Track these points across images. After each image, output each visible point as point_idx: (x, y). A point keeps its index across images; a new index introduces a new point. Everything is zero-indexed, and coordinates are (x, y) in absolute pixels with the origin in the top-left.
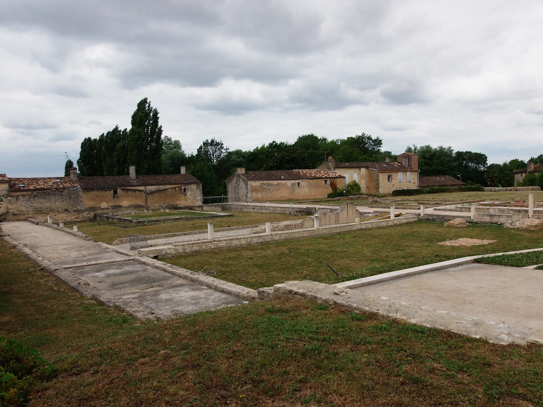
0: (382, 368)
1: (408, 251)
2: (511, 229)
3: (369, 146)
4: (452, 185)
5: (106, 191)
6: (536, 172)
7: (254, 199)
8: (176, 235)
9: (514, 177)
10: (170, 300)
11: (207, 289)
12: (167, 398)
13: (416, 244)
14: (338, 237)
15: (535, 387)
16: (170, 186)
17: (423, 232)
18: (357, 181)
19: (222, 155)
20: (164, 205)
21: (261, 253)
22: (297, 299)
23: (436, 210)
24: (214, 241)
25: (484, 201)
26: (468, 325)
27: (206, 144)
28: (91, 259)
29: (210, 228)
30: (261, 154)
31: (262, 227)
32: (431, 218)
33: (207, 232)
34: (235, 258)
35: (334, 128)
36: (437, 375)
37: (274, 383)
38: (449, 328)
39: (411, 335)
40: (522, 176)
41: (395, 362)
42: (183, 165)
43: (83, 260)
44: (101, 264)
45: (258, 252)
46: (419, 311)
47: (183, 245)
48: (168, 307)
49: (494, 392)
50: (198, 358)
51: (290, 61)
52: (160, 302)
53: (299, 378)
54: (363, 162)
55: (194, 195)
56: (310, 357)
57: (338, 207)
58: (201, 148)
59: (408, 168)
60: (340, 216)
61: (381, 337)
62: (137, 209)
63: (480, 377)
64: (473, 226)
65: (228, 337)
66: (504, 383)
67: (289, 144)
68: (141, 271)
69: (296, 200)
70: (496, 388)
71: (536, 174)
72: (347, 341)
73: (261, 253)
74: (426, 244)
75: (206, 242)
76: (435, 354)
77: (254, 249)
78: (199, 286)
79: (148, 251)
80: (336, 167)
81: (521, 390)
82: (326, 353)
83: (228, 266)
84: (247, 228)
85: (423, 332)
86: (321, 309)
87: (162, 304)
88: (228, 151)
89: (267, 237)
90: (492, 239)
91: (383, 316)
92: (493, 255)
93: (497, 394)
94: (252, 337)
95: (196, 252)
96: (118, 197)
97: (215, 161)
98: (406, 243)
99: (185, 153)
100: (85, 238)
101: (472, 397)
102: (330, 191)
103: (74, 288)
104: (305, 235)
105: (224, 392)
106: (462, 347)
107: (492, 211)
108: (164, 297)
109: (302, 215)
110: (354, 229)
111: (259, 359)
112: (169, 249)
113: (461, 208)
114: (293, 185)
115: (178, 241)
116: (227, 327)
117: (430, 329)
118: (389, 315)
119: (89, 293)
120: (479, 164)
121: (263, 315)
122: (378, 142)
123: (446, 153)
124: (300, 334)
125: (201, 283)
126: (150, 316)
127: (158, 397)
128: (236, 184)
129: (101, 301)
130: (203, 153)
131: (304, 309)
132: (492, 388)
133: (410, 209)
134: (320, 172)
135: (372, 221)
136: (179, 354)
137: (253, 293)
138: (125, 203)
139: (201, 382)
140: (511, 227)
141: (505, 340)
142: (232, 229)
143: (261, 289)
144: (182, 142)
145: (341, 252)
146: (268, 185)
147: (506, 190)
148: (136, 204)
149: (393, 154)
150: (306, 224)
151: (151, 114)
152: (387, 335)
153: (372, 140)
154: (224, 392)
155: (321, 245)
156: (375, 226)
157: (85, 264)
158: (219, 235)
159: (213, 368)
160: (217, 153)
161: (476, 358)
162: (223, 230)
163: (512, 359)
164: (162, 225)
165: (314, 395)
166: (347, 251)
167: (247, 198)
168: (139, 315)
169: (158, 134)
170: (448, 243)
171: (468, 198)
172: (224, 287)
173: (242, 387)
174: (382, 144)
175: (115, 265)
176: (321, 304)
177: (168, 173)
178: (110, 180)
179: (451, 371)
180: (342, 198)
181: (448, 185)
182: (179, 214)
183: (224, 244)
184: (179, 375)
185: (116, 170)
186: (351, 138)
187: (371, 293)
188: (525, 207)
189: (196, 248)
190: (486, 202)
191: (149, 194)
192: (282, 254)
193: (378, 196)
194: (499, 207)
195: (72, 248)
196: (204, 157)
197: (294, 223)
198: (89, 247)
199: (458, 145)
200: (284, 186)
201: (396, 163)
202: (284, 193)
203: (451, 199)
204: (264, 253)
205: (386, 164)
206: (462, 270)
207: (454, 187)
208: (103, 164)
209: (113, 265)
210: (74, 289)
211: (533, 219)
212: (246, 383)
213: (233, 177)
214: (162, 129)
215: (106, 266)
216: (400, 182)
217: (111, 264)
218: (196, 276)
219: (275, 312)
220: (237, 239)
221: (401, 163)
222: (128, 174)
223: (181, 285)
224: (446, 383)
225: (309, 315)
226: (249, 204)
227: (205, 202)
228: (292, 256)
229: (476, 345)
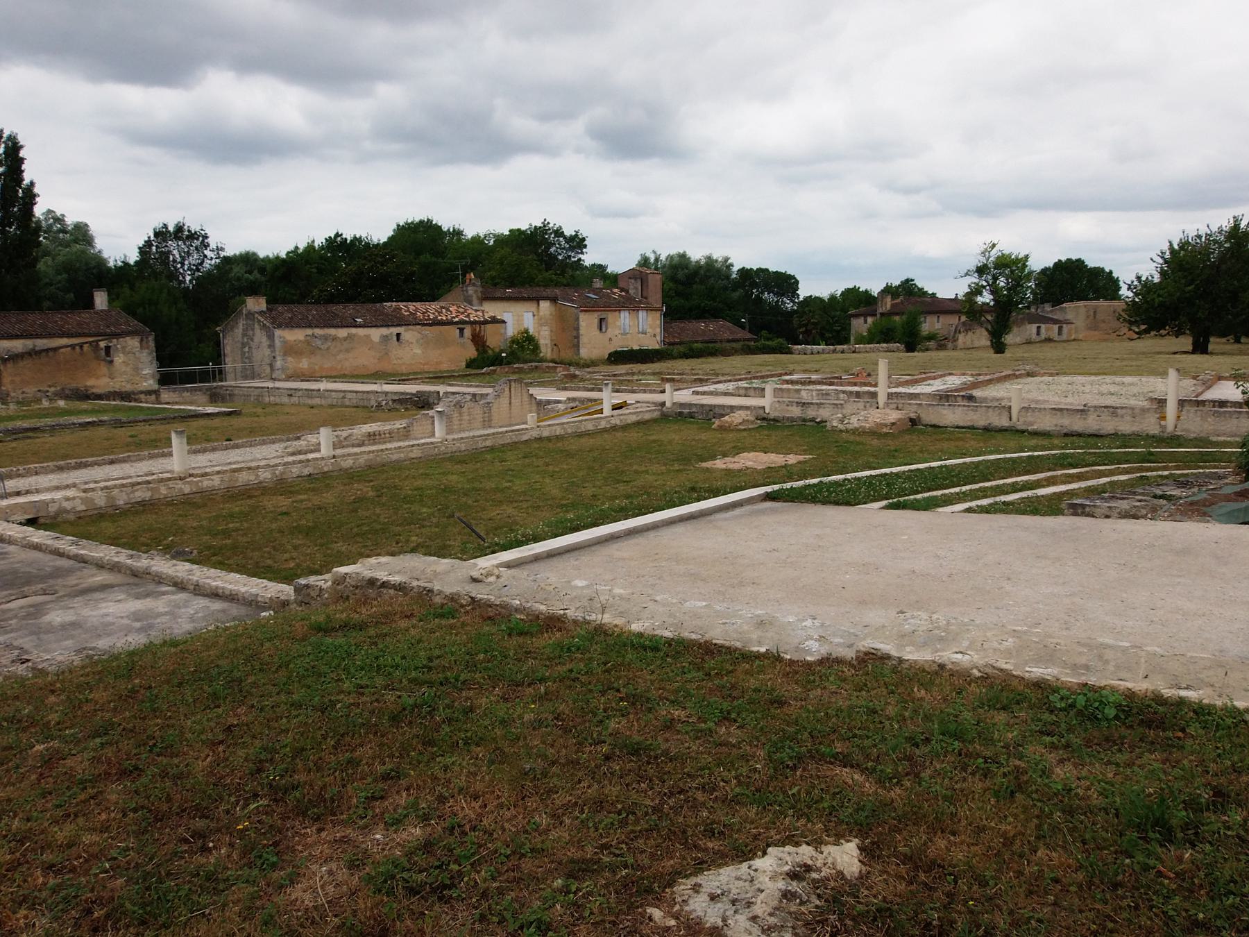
0: (566, 731)
1: (639, 483)
3: (558, 250)
4: (729, 341)
6: (897, 314)
7: (289, 372)
8: (86, 465)
10: (74, 625)
11: (173, 593)
12: (48, 857)
13: (655, 468)
15: (868, 737)
16: (65, 341)
17: (670, 442)
18: (531, 331)
19: (207, 264)
20: (52, 389)
21: (309, 500)
22: (387, 597)
23: (697, 393)
24: (191, 475)
25: (791, 374)
26: (746, 628)
27: (161, 234)
29: (178, 444)
30: (307, 262)
31: (312, 439)
32: (686, 411)
33: (171, 454)
35: (480, 206)
36: (679, 732)
37: (324, 788)
38: (707, 637)
39: (630, 656)
40: (866, 322)
41: (595, 715)
42: (100, 286)
45: (302, 497)
46: (651, 605)
47: (106, 488)
48: (69, 643)
49: (783, 755)
50: (134, 751)
51: (375, 36)
52: (48, 632)
53: (381, 769)
54: (546, 286)
55: (133, 364)
56: (410, 722)
57: (490, 390)
58: (148, 243)
59: (640, 302)
60: (494, 409)
61: (568, 666)
63: (762, 728)
64: (769, 428)
65: (215, 696)
66: (806, 735)
67: (375, 241)
69: (394, 375)
70: (790, 748)
71: (897, 318)
72: (495, 681)
73: (309, 500)
75: (169, 479)
76: (677, 691)
77: (291, 492)
78: (151, 587)
79: (8, 506)
80: (486, 298)
81: (839, 747)
82: (447, 711)
83: (226, 533)
85: (655, 649)
86: (442, 616)
87: (51, 637)
88: (222, 254)
89: (323, 463)
90: (805, 452)
91: (575, 622)
92: (801, 483)
93: (791, 758)
94: (275, 690)
97: (188, 278)
98: (635, 467)
99: (105, 255)
101: (744, 771)
102: (472, 352)
104: (413, 455)
105: (200, 824)
106: (731, 672)
107: (805, 396)
108: (59, 619)
109: (406, 409)
110: (525, 438)
111: (288, 739)
112: (68, 499)
113: (746, 388)
114: (385, 338)
115: (93, 478)
116: (214, 672)
117: (669, 642)
120: (783, 295)
121: (303, 639)
122: (578, 243)
123: (719, 271)
124: (390, 674)
125: (159, 579)
126: (21, 669)
127: (25, 856)
128: (244, 335)
131: (401, 618)
132: (783, 747)
133: (645, 392)
134: (448, 310)
135: (565, 420)
136: (86, 749)
137: (286, 591)
139: (143, 807)
140: (841, 427)
141: (814, 650)
142: (237, 447)
143: (303, 581)
144: (95, 229)
145: (496, 490)
146: (326, 338)
147: (834, 351)
149: (609, 270)
150: (417, 429)
152: (581, 660)
153: (565, 237)
154: (200, 824)
155: (451, 477)
156: (569, 431)
158: (202, 461)
159: (175, 771)
160: (194, 258)
161: (756, 690)
162: (214, 449)
163: (825, 688)
164: (48, 440)
165: (415, 806)
166: (509, 488)
169: (25, 204)
170: (719, 464)
171: (759, 368)
172: (219, 583)
173: (246, 805)
174: (585, 246)
176: (442, 606)
177: (59, 306)
179: (705, 722)
180: (498, 368)
181: (721, 341)
183: (216, 481)
184: (82, 797)
186: (519, 230)
187: (551, 575)
188: (871, 385)
189: (141, 494)
190: (795, 377)
192: (360, 500)
193: (578, 365)
194: (818, 387)
196: (159, 268)
197: (388, 427)
199: (744, 256)
200: (364, 342)
202: (364, 358)
203: (727, 370)
204: (316, 500)
205: (595, 291)
206: (741, 516)
207: (734, 345)
211: (888, 411)
212: (256, 796)
214: (36, 190)
216: (625, 334)
218: (143, 562)
219: (333, 629)
220: (250, 468)
221: (627, 292)
223: (104, 588)
224: (694, 748)
225: (413, 632)
226: (278, 384)
228: (384, 505)
229: (759, 666)
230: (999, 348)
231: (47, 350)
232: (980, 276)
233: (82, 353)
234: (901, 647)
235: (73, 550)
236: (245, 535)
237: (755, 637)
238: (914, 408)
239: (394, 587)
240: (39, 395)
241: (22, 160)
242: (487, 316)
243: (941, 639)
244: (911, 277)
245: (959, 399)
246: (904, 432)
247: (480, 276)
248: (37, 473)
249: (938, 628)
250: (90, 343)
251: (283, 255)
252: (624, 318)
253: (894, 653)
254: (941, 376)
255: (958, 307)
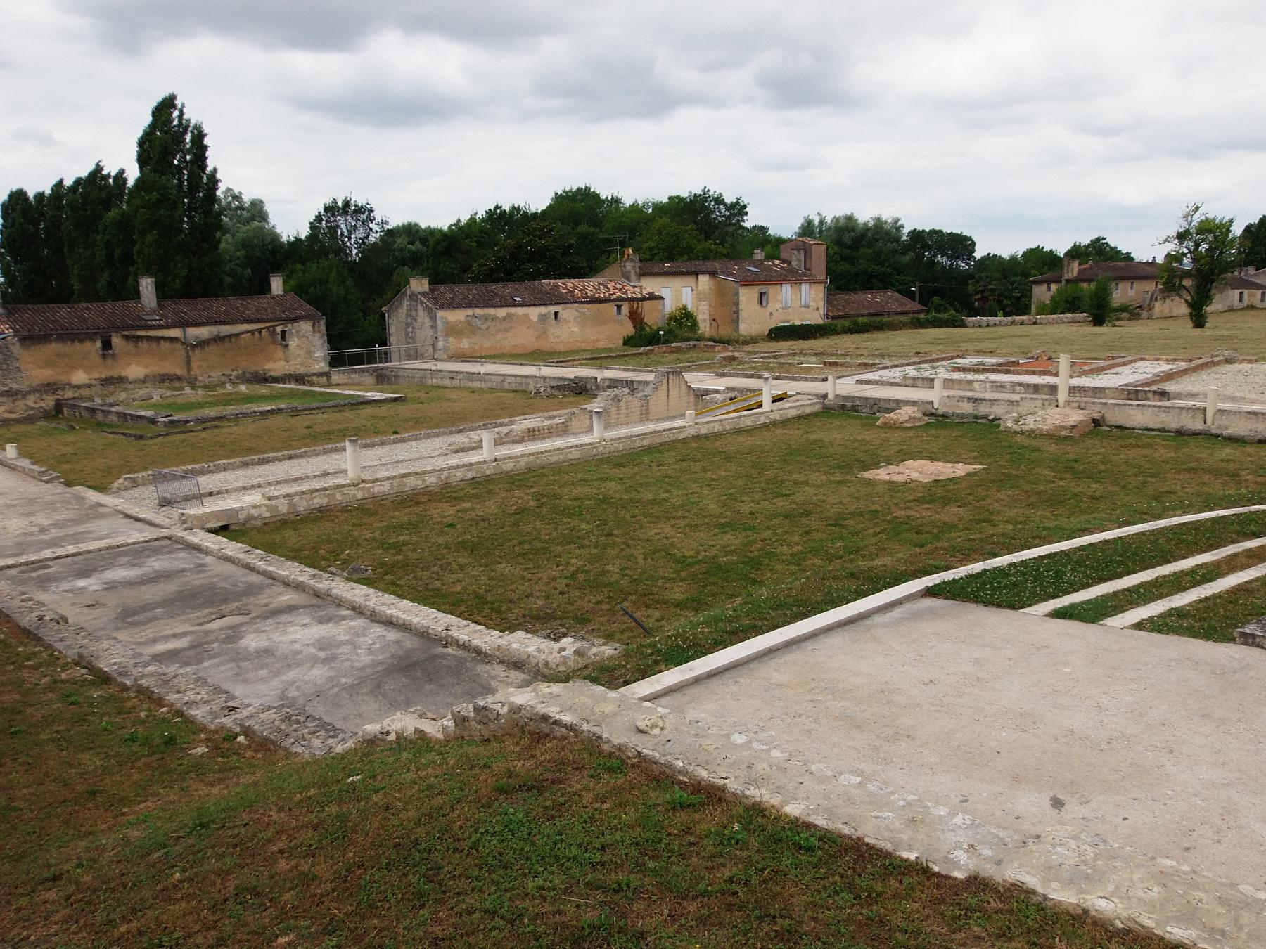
1: (798, 497)
2: (1016, 432)
4: (897, 313)
5: (81, 341)
6: (1084, 281)
7: (451, 352)
9: (1031, 291)
10: (267, 652)
11: (352, 618)
13: (815, 477)
14: (646, 458)
16: (245, 327)
18: (689, 307)
20: (234, 373)
24: (363, 481)
25: (963, 357)
26: (897, 824)
27: (330, 209)
28: (62, 539)
31: (475, 435)
34: (414, 527)
35: (640, 169)
38: (859, 833)
40: (1049, 289)
43: (41, 542)
44: (89, 552)
45: (467, 505)
47: (288, 495)
52: (245, 659)
54: (705, 258)
55: (306, 346)
57: (650, 377)
58: (319, 218)
60: (651, 402)
62: (167, 384)
67: (533, 210)
68: (190, 570)
71: (1085, 285)
73: (473, 509)
74: (838, 477)
75: (344, 486)
78: (332, 610)
80: (644, 273)
83: (397, 547)
84: (437, 435)
88: (386, 227)
89: (485, 466)
95: (320, 509)
96: (114, 357)
97: (355, 251)
98: (795, 476)
99: (278, 230)
100: (40, 477)
102: (629, 329)
103: (30, 632)
108: (253, 644)
109: (564, 396)
110: (683, 436)
114: (543, 317)
118: (748, 793)
119: (70, 646)
120: (958, 258)
122: (739, 209)
123: (888, 233)
125: (339, 602)
126: (228, 721)
128: (408, 315)
129: (101, 670)
130: (324, 239)
134: (606, 287)
138: (135, 371)
142: (403, 440)
145: (654, 502)
146: (486, 318)
147: (1013, 323)
148: (165, 371)
150: (575, 424)
151: (188, 138)
153: (725, 205)
156: (728, 427)
157: (47, 553)
162: (382, 444)
164: (231, 430)
166: (666, 500)
167: (434, 350)
168: (199, 713)
175: (125, 554)
178: (89, 312)
180: (656, 348)
182: (271, 398)
183: (386, 487)
185: (103, 279)
186: (678, 197)
189: (319, 501)
191: (194, 347)
192: (522, 511)
195: (9, 506)
198: (53, 503)
199: (915, 213)
200: (523, 321)
201: (778, 262)
202: (523, 338)
207: (903, 318)
208: (69, 262)
209: (119, 555)
210: (29, 635)
211: (1068, 411)
213: (401, 299)
214: (219, 176)
215: (104, 559)
216: (786, 308)
217: (113, 555)
218: (324, 583)
221: (789, 263)
222: (136, 294)
223: (291, 609)
227: (336, 362)
230: (1199, 320)
231: (230, 336)
232: (1181, 243)
233: (261, 339)
234: (1046, 881)
235: (262, 565)
236: (415, 550)
237: (905, 837)
238: (1098, 408)
239: (565, 726)
240: (223, 378)
241: (206, 148)
242: (645, 293)
243: (1088, 878)
244: (1102, 235)
245: (1150, 395)
246: (1085, 435)
247: (636, 250)
248: (225, 469)
249: (1085, 863)
250: (267, 328)
251: (445, 228)
252: (785, 293)
253: (1040, 890)
254: (1131, 362)
255: (1156, 272)
